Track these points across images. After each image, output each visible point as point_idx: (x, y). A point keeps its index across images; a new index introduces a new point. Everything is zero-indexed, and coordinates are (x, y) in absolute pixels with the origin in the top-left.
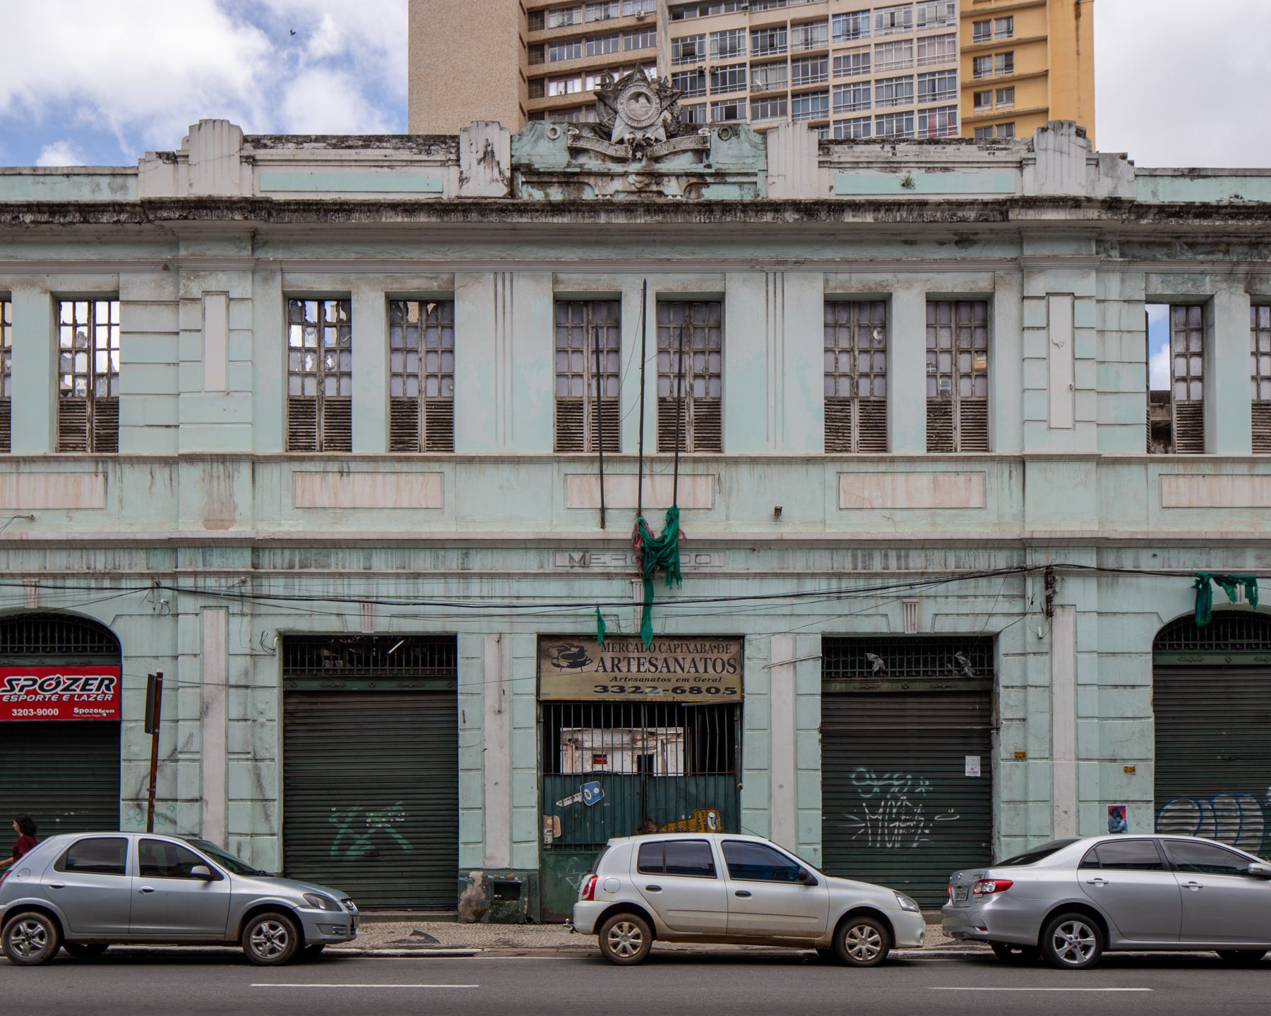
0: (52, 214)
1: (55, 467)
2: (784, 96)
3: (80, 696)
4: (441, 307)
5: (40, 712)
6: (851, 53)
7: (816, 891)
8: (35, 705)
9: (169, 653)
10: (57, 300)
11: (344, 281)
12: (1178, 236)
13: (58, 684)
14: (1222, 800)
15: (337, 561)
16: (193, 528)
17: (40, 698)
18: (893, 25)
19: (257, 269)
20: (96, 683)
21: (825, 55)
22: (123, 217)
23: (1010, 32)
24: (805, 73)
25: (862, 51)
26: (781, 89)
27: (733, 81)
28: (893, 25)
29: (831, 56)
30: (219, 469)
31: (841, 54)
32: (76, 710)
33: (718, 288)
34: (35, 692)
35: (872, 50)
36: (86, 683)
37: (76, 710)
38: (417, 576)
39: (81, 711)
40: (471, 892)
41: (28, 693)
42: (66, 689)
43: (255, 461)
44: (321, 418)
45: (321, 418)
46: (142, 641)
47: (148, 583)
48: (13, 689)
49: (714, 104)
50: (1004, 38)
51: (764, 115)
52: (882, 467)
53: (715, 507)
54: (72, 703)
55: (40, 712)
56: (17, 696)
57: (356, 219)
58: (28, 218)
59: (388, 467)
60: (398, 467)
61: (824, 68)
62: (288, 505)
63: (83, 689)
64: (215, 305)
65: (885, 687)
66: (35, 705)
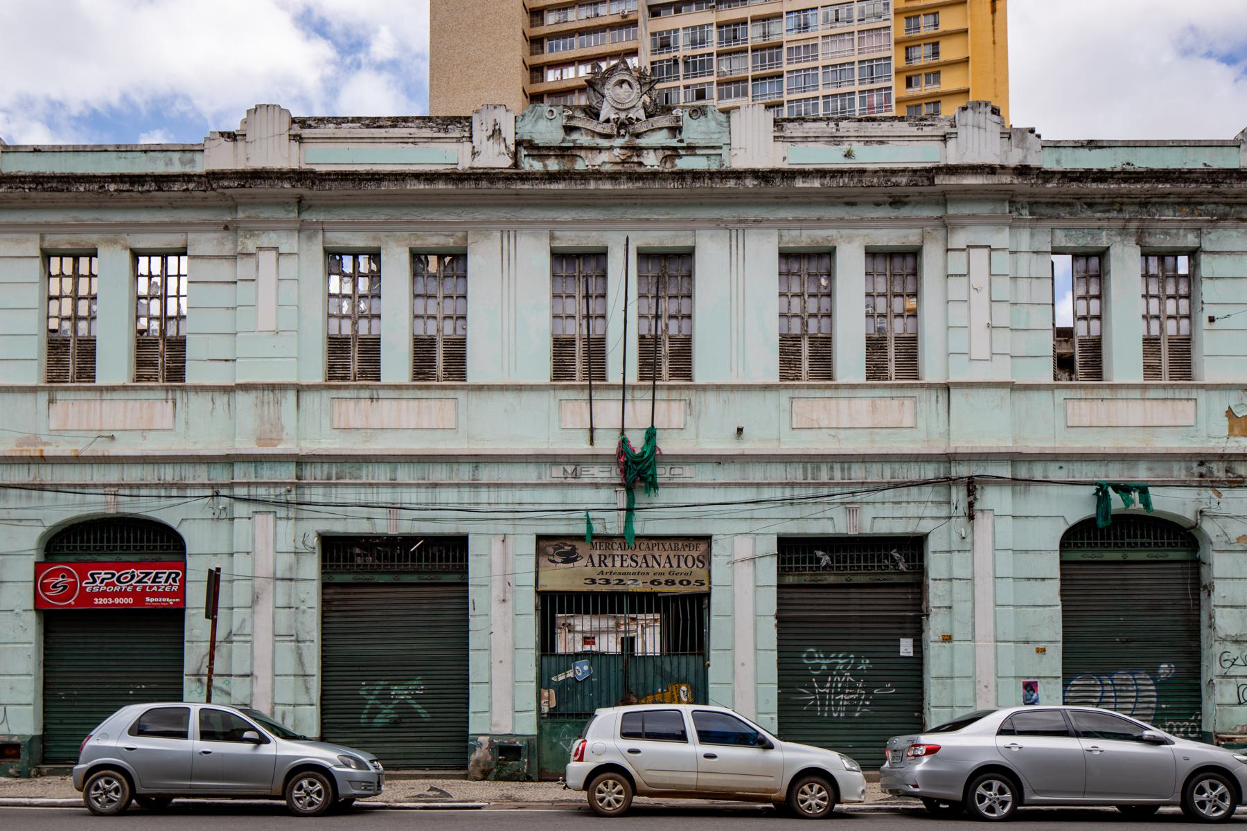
0: (132, 184)
2: (745, 80)
3: (151, 587)
4: (456, 259)
5: (117, 601)
6: (802, 43)
7: (771, 754)
9: (226, 550)
10: (136, 255)
11: (374, 239)
12: (1078, 197)
14: (1121, 676)
16: (248, 446)
18: (837, 20)
19: (302, 228)
20: (165, 576)
21: (780, 46)
22: (191, 186)
23: (936, 25)
24: (763, 60)
25: (811, 42)
26: (743, 74)
27: (702, 68)
28: (837, 20)
29: (785, 46)
31: (793, 45)
32: (148, 599)
33: (689, 243)
34: (113, 584)
35: (820, 41)
36: (156, 576)
37: (148, 599)
38: (435, 485)
39: (152, 600)
40: (479, 754)
41: (107, 585)
42: (140, 581)
43: (299, 389)
44: (355, 353)
45: (355, 353)
46: (203, 542)
47: (209, 492)
48: (95, 581)
49: (686, 87)
50: (932, 31)
51: (729, 96)
52: (828, 393)
54: (144, 593)
55: (117, 601)
57: (386, 186)
58: (112, 187)
59: (411, 394)
60: (419, 394)
61: (779, 57)
62: (327, 425)
63: (154, 581)
64: (267, 259)
65: (831, 579)
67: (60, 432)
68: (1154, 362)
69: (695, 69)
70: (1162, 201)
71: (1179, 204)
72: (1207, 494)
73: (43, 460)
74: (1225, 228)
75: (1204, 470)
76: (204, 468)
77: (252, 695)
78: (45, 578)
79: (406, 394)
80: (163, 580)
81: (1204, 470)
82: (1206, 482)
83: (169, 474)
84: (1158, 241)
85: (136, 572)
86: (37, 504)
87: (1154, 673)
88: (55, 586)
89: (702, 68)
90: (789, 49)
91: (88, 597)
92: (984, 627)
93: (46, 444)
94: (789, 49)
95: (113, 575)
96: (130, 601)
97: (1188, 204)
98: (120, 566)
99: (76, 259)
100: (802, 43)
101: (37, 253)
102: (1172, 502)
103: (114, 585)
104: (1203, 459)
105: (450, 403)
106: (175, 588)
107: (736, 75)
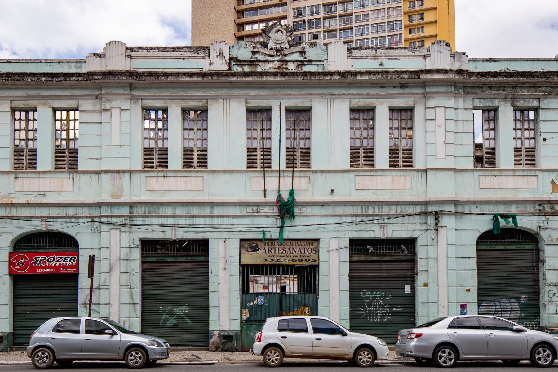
1: (53, 175)
2: (336, 30)
3: (63, 264)
4: (203, 112)
5: (47, 270)
7: (346, 338)
8: (46, 268)
10: (55, 110)
11: (165, 103)
12: (485, 84)
13: (54, 259)
14: (503, 302)
15: (163, 211)
17: (47, 265)
18: (377, 3)
20: (69, 259)
21: (352, 15)
23: (422, 5)
24: (344, 21)
26: (335, 28)
27: (316, 25)
28: (377, 3)
30: (117, 175)
31: (358, 14)
32: (61, 269)
33: (309, 105)
34: (45, 262)
35: (370, 12)
36: (65, 259)
39: (63, 270)
41: (42, 263)
42: (58, 261)
43: (131, 172)
44: (156, 156)
45: (156, 156)
46: (87, 243)
47: (89, 220)
48: (37, 261)
49: (309, 33)
50: (420, 8)
51: (329, 38)
53: (308, 189)
54: (60, 267)
55: (47, 270)
56: (38, 264)
57: (170, 79)
58: (44, 79)
60: (186, 174)
61: (351, 20)
63: (64, 261)
64: (116, 112)
65: (374, 258)
66: (46, 268)
67: (20, 193)
68: (518, 159)
69: (313, 25)
70: (522, 85)
71: (530, 87)
72: (543, 219)
73: (12, 205)
74: (550, 98)
75: (541, 208)
76: (87, 209)
77: (110, 313)
78: (13, 260)
79: (180, 174)
80: (68, 260)
81: (541, 208)
82: (542, 213)
83: (71, 211)
84: (521, 104)
85: (56, 257)
86: (8, 225)
87: (518, 300)
88: (18, 264)
89: (316, 25)
90: (356, 16)
91: (33, 268)
92: (443, 279)
93: (13, 198)
94: (356, 16)
95: (45, 258)
96: (53, 270)
97: (534, 87)
98: (48, 254)
99: (27, 112)
100: (362, 14)
101: (9, 109)
102: (527, 223)
103: (46, 263)
104: (541, 203)
105: (200, 179)
106: (74, 264)
107: (332, 28)
